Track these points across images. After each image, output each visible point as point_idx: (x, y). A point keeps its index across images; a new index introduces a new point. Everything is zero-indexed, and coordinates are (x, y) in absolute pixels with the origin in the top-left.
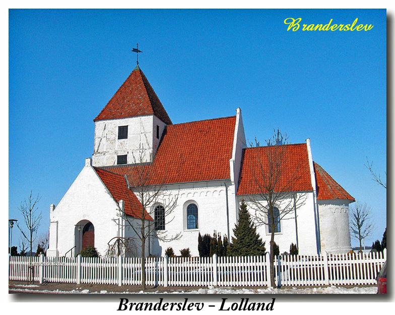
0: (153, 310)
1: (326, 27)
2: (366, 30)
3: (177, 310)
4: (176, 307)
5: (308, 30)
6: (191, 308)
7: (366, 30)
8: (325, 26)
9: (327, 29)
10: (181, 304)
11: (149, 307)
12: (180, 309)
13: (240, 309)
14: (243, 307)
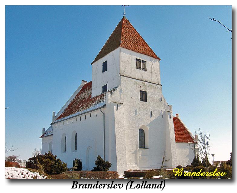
0: (93, 188)
1: (198, 174)
2: (222, 176)
3: (107, 188)
4: (106, 186)
5: (187, 176)
6: (115, 187)
7: (222, 176)
8: (198, 173)
9: (198, 175)
10: (110, 184)
11: (90, 186)
12: (109, 188)
13: (141, 188)
14: (143, 186)
